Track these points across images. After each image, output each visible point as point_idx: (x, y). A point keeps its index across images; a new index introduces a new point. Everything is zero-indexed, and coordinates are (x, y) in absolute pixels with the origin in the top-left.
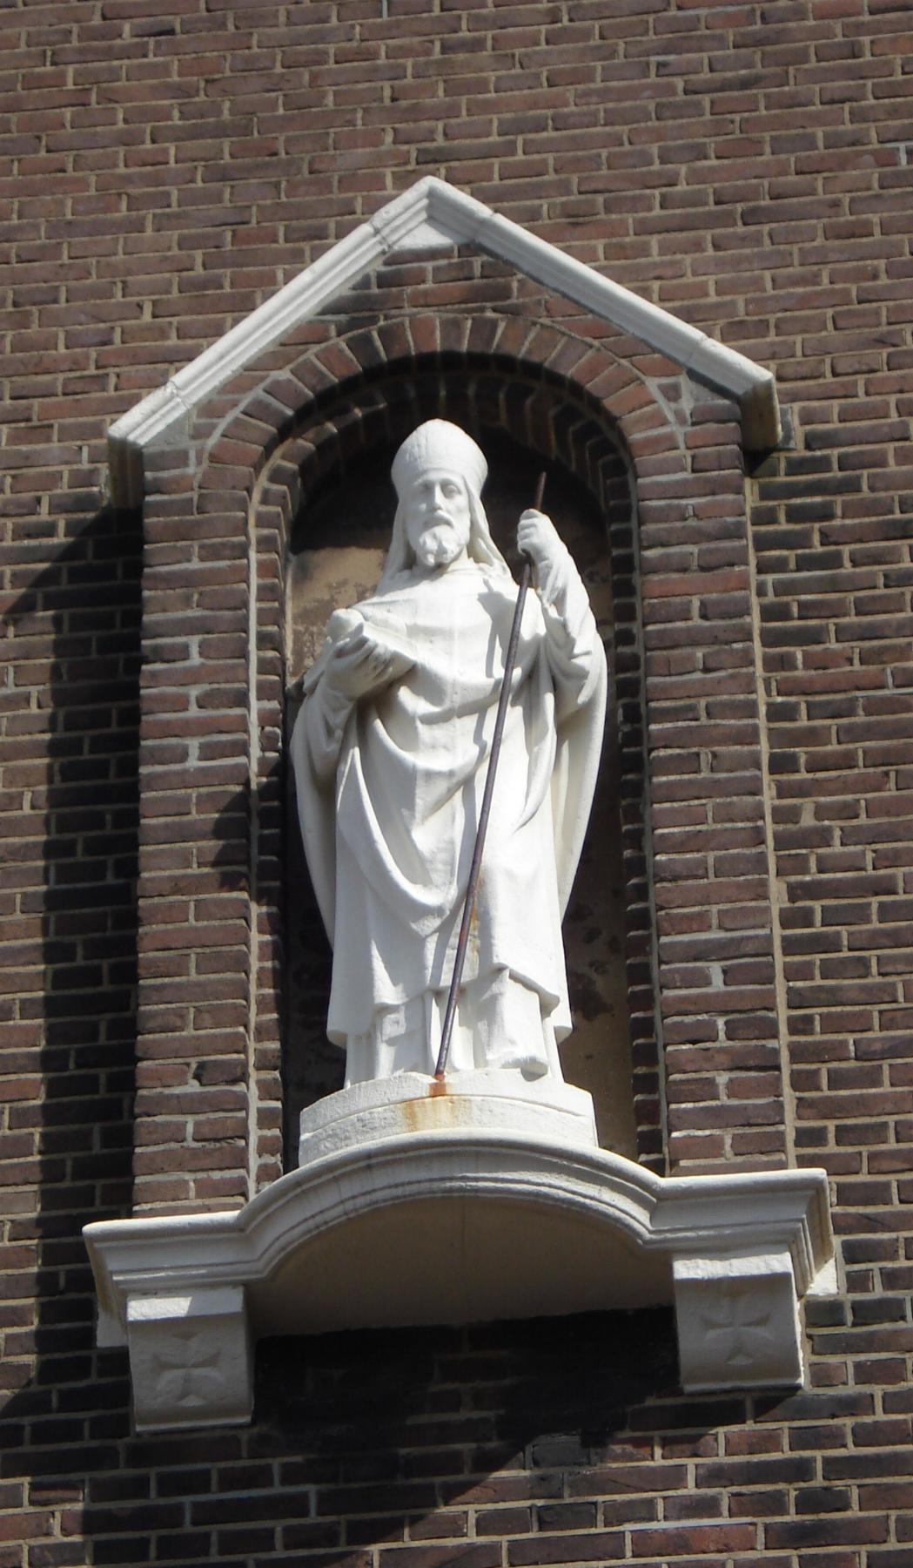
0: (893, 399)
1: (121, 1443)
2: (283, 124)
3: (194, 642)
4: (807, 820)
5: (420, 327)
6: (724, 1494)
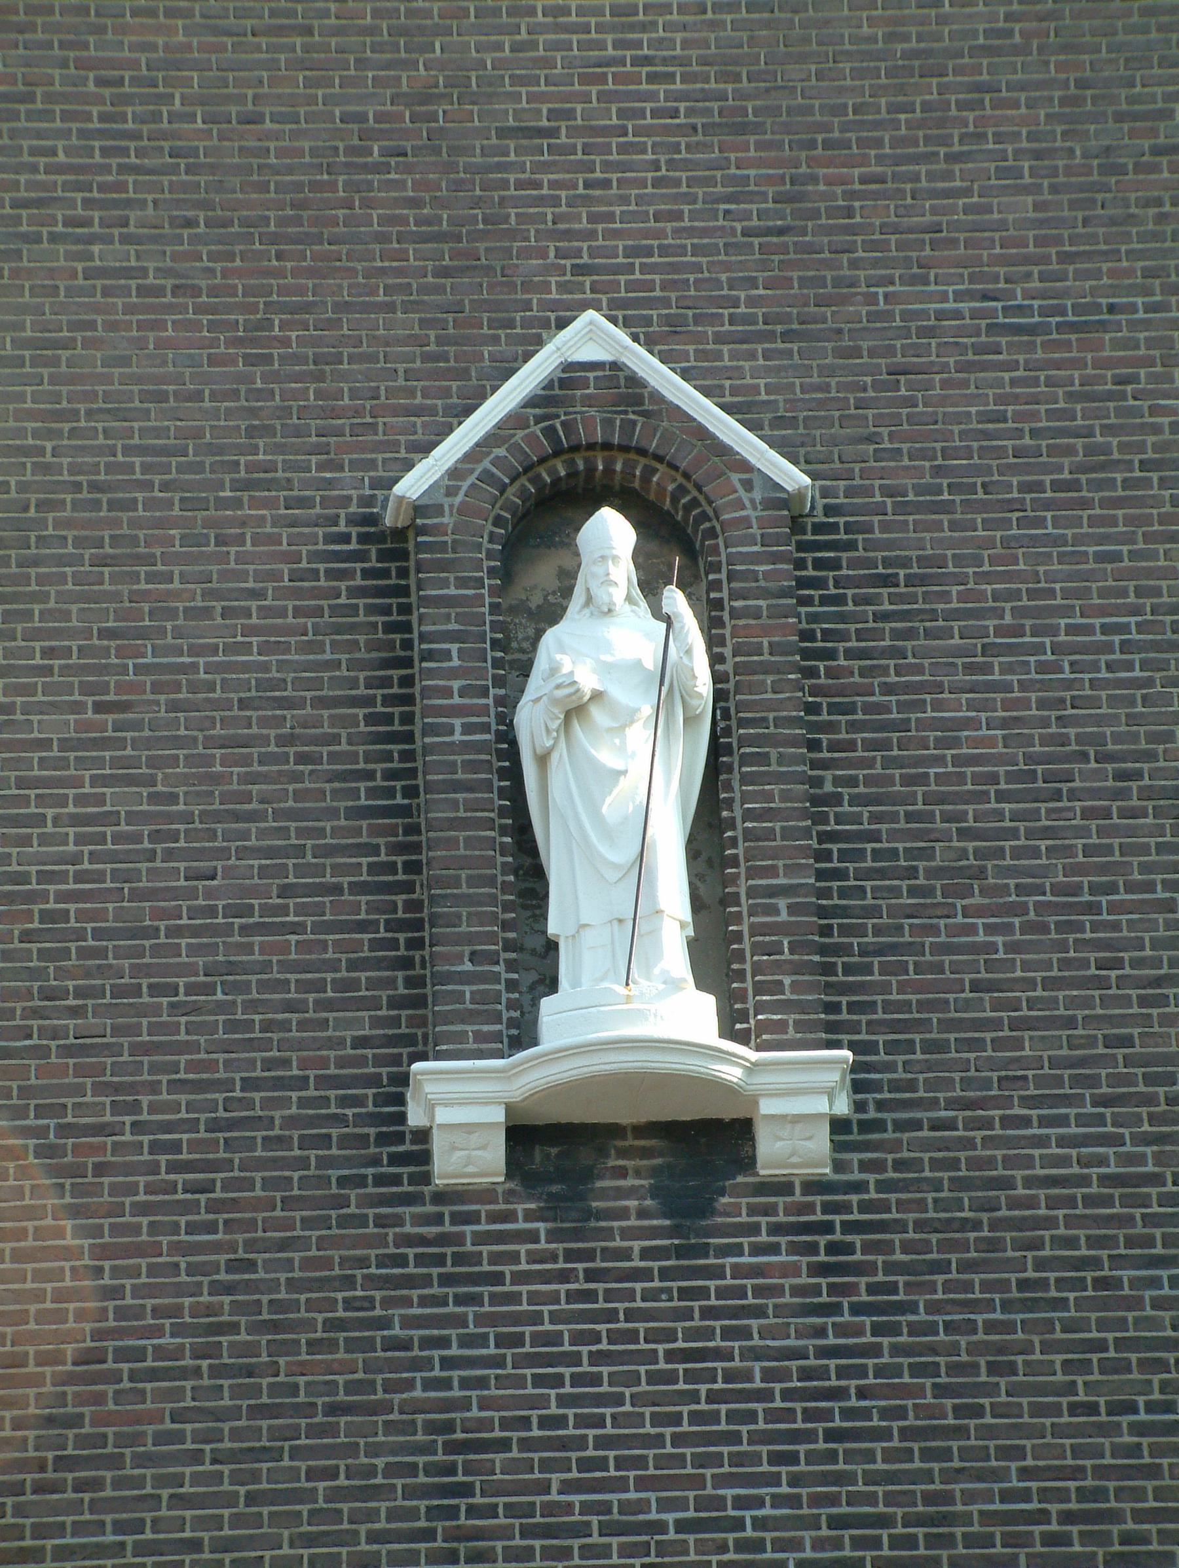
0: (877, 483)
1: (426, 1189)
2: (484, 235)
3: (454, 648)
4: (828, 787)
5: (588, 422)
6: (783, 1240)
